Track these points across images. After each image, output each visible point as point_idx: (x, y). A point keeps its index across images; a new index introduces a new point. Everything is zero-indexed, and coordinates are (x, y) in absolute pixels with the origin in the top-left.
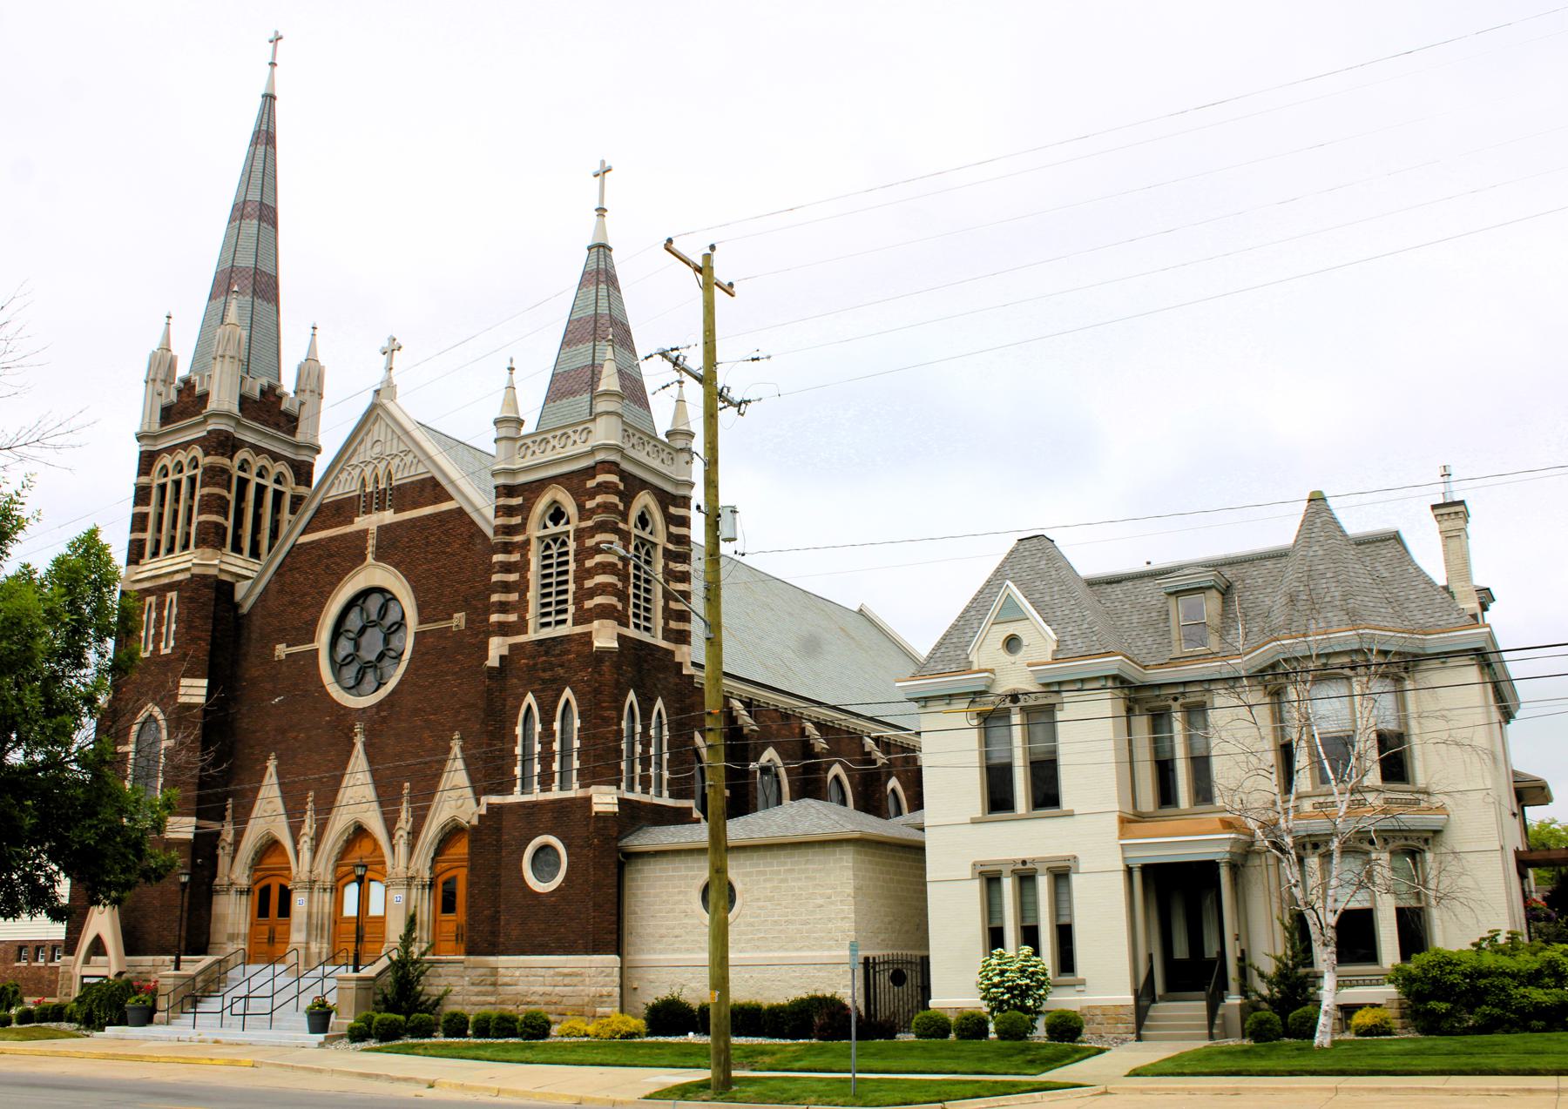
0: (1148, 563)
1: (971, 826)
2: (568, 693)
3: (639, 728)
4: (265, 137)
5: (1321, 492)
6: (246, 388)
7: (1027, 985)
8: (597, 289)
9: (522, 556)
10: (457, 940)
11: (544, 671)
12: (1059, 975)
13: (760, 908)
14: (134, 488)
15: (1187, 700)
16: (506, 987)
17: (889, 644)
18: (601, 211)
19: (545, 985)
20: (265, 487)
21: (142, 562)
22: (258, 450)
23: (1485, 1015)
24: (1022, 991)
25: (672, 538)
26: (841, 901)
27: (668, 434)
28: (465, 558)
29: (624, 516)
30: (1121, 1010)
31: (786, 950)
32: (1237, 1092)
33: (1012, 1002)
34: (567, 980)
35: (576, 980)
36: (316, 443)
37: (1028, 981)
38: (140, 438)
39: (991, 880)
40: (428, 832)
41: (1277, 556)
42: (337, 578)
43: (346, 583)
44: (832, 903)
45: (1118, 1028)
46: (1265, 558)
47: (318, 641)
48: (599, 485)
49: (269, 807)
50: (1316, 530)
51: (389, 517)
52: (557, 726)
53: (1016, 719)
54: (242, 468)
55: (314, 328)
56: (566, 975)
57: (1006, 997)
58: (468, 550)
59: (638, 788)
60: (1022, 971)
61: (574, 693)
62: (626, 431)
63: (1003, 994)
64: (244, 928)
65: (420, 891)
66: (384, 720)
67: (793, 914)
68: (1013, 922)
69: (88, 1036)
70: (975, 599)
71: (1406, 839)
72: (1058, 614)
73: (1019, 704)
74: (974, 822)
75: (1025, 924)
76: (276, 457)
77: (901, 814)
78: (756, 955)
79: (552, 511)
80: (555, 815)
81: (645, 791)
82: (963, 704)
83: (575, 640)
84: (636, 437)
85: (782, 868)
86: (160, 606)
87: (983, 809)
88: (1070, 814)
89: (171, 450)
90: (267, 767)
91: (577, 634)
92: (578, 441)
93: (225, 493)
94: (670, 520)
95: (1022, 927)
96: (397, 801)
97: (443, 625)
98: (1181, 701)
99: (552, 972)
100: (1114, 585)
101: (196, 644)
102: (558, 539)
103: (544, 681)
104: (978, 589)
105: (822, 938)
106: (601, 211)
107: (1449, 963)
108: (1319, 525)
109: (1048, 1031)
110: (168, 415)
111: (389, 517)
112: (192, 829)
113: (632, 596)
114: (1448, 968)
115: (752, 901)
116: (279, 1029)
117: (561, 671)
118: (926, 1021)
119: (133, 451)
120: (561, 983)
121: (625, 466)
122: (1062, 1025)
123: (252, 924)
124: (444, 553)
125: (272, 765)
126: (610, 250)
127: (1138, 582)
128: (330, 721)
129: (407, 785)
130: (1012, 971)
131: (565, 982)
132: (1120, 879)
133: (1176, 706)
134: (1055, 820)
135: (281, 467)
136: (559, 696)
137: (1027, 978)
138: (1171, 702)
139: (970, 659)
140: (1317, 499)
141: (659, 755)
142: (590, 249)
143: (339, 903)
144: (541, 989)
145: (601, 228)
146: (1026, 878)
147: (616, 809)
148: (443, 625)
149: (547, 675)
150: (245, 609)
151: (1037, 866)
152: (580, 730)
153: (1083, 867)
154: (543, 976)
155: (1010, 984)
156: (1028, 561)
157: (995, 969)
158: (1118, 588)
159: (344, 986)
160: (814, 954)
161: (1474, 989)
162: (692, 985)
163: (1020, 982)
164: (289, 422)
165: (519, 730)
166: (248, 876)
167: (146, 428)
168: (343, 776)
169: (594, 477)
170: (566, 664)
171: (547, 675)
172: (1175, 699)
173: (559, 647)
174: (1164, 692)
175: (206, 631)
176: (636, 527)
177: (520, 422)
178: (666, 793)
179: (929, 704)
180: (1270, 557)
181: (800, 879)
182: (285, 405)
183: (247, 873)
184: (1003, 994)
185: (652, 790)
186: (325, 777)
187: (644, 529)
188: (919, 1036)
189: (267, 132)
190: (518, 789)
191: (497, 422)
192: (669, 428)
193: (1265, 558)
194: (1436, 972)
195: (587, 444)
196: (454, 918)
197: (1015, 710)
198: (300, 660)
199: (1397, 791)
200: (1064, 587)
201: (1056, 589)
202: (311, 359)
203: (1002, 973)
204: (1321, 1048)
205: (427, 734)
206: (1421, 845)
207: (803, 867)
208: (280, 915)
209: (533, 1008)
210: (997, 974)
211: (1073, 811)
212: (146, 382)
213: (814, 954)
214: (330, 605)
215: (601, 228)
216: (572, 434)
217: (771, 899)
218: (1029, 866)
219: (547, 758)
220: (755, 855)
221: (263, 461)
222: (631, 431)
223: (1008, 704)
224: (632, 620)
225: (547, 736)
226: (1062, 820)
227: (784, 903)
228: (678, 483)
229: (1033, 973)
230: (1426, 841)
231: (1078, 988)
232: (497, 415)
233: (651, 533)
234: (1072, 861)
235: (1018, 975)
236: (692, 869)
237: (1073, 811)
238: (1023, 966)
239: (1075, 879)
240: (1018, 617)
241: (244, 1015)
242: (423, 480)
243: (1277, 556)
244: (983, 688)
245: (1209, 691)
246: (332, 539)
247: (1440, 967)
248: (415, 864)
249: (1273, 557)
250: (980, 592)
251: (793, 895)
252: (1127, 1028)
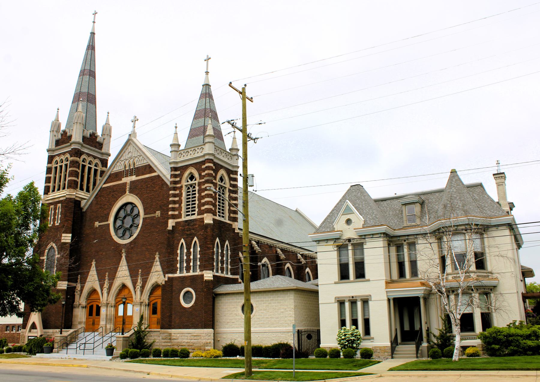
0: (396, 194)
1: (334, 284)
2: (195, 239)
3: (220, 251)
4: (91, 47)
5: (455, 170)
6: (85, 134)
7: (354, 339)
8: (206, 99)
9: (180, 191)
10: (157, 324)
11: (187, 231)
12: (365, 336)
13: (262, 313)
14: (46, 168)
15: (409, 241)
16: (174, 340)
17: (306, 222)
18: (207, 73)
19: (188, 339)
20: (91, 168)
21: (49, 193)
22: (89, 155)
23: (512, 350)
24: (352, 341)
25: (231, 185)
26: (290, 310)
27: (230, 150)
28: (160, 192)
29: (215, 178)
30: (386, 348)
31: (271, 327)
32: (426, 376)
34: (195, 338)
35: (198, 337)
36: (109, 153)
37: (354, 338)
38: (48, 151)
39: (341, 303)
40: (147, 286)
41: (440, 192)
42: (116, 199)
43: (119, 201)
44: (286, 311)
45: (385, 354)
46: (436, 192)
47: (110, 221)
48: (206, 167)
49: (93, 278)
51: (134, 178)
52: (192, 250)
53: (350, 247)
54: (83, 161)
55: (108, 113)
56: (195, 336)
57: (347, 343)
58: (161, 189)
59: (220, 271)
60: (352, 334)
61: (198, 239)
62: (215, 148)
63: (345, 342)
64: (84, 320)
65: (145, 307)
66: (132, 248)
67: (273, 315)
68: (349, 318)
69: (30, 357)
70: (336, 206)
71: (484, 289)
72: (364, 211)
73: (351, 243)
74: (336, 283)
75: (353, 318)
76: (95, 158)
77: (310, 280)
78: (260, 329)
79: (190, 176)
80: (191, 281)
81: (222, 272)
82: (332, 243)
83: (198, 220)
84: (219, 151)
85: (269, 299)
86: (55, 209)
87: (339, 279)
88: (369, 280)
89: (59, 155)
90: (92, 264)
91: (199, 218)
92: (199, 152)
93: (77, 170)
94: (231, 179)
95: (352, 319)
96: (137, 276)
97: (153, 215)
98: (407, 241)
99: (190, 335)
100: (384, 202)
101: (67, 222)
102: (192, 186)
103: (187, 235)
104: (337, 203)
105: (283, 323)
106: (207, 73)
107: (499, 332)
110: (58, 143)
111: (134, 178)
112: (66, 286)
113: (217, 205)
114: (499, 334)
115: (259, 310)
116: (96, 354)
117: (193, 231)
118: (319, 352)
119: (46, 155)
120: (193, 339)
121: (215, 160)
122: (366, 353)
123: (87, 318)
124: (153, 190)
125: (94, 263)
126: (210, 86)
127: (392, 201)
128: (114, 249)
129: (140, 270)
130: (348, 335)
131: (195, 338)
132: (386, 303)
133: (405, 243)
134: (363, 282)
135: (97, 161)
136: (192, 240)
137: (354, 337)
138: (403, 242)
139: (334, 227)
140: (453, 172)
141: (227, 260)
142: (203, 86)
143: (117, 311)
144: (186, 341)
145: (207, 79)
146: (353, 303)
147: (212, 279)
148: (153, 215)
149: (188, 233)
150: (84, 210)
151: (357, 298)
152: (200, 251)
153: (373, 299)
154: (187, 336)
155: (348, 339)
156: (354, 193)
157: (343, 334)
158: (385, 203)
159: (118, 340)
160: (280, 328)
161: (507, 341)
162: (238, 339)
163: (351, 338)
164: (100, 145)
165: (179, 252)
166: (85, 302)
167: (50, 147)
168: (118, 267)
169: (204, 164)
170: (195, 229)
171: (188, 233)
172: (405, 241)
173: (193, 223)
174: (401, 238)
175: (71, 217)
176: (219, 181)
177: (179, 145)
178: (229, 273)
179: (320, 242)
180: (437, 192)
181: (275, 303)
182: (98, 140)
183: (85, 301)
184: (345, 342)
185: (225, 272)
186: (112, 268)
187: (222, 182)
188: (316, 357)
189: (92, 45)
190: (178, 272)
191: (171, 145)
192: (230, 147)
193: (436, 192)
194: (494, 335)
195: (202, 153)
196: (156, 316)
198: (103, 227)
199: (481, 273)
200: (366, 202)
201: (364, 203)
202: (107, 124)
203: (345, 335)
204: (455, 361)
205: (147, 253)
206: (489, 291)
207: (277, 299)
208: (97, 315)
209: (183, 347)
210: (344, 336)
211: (369, 279)
212: (50, 132)
213: (280, 328)
214: (114, 209)
215: (207, 79)
216: (197, 149)
217: (265, 310)
218: (354, 298)
219: (188, 261)
220: (260, 294)
221: (91, 159)
222: (217, 148)
223: (347, 243)
224: (218, 213)
225: (188, 254)
226: (366, 282)
227: (270, 311)
228: (233, 166)
229: (356, 335)
231: (371, 340)
232: (171, 143)
233: (224, 184)
234: (369, 296)
235: (351, 336)
236: (238, 299)
237: (369, 279)
238: (352, 333)
239: (370, 303)
240: (350, 213)
241: (84, 349)
242: (146, 165)
243: (440, 192)
244: (338, 237)
245: (416, 238)
246: (114, 186)
248: (143, 298)
249: (438, 192)
250: (338, 204)
251: (273, 308)
252: (388, 354)
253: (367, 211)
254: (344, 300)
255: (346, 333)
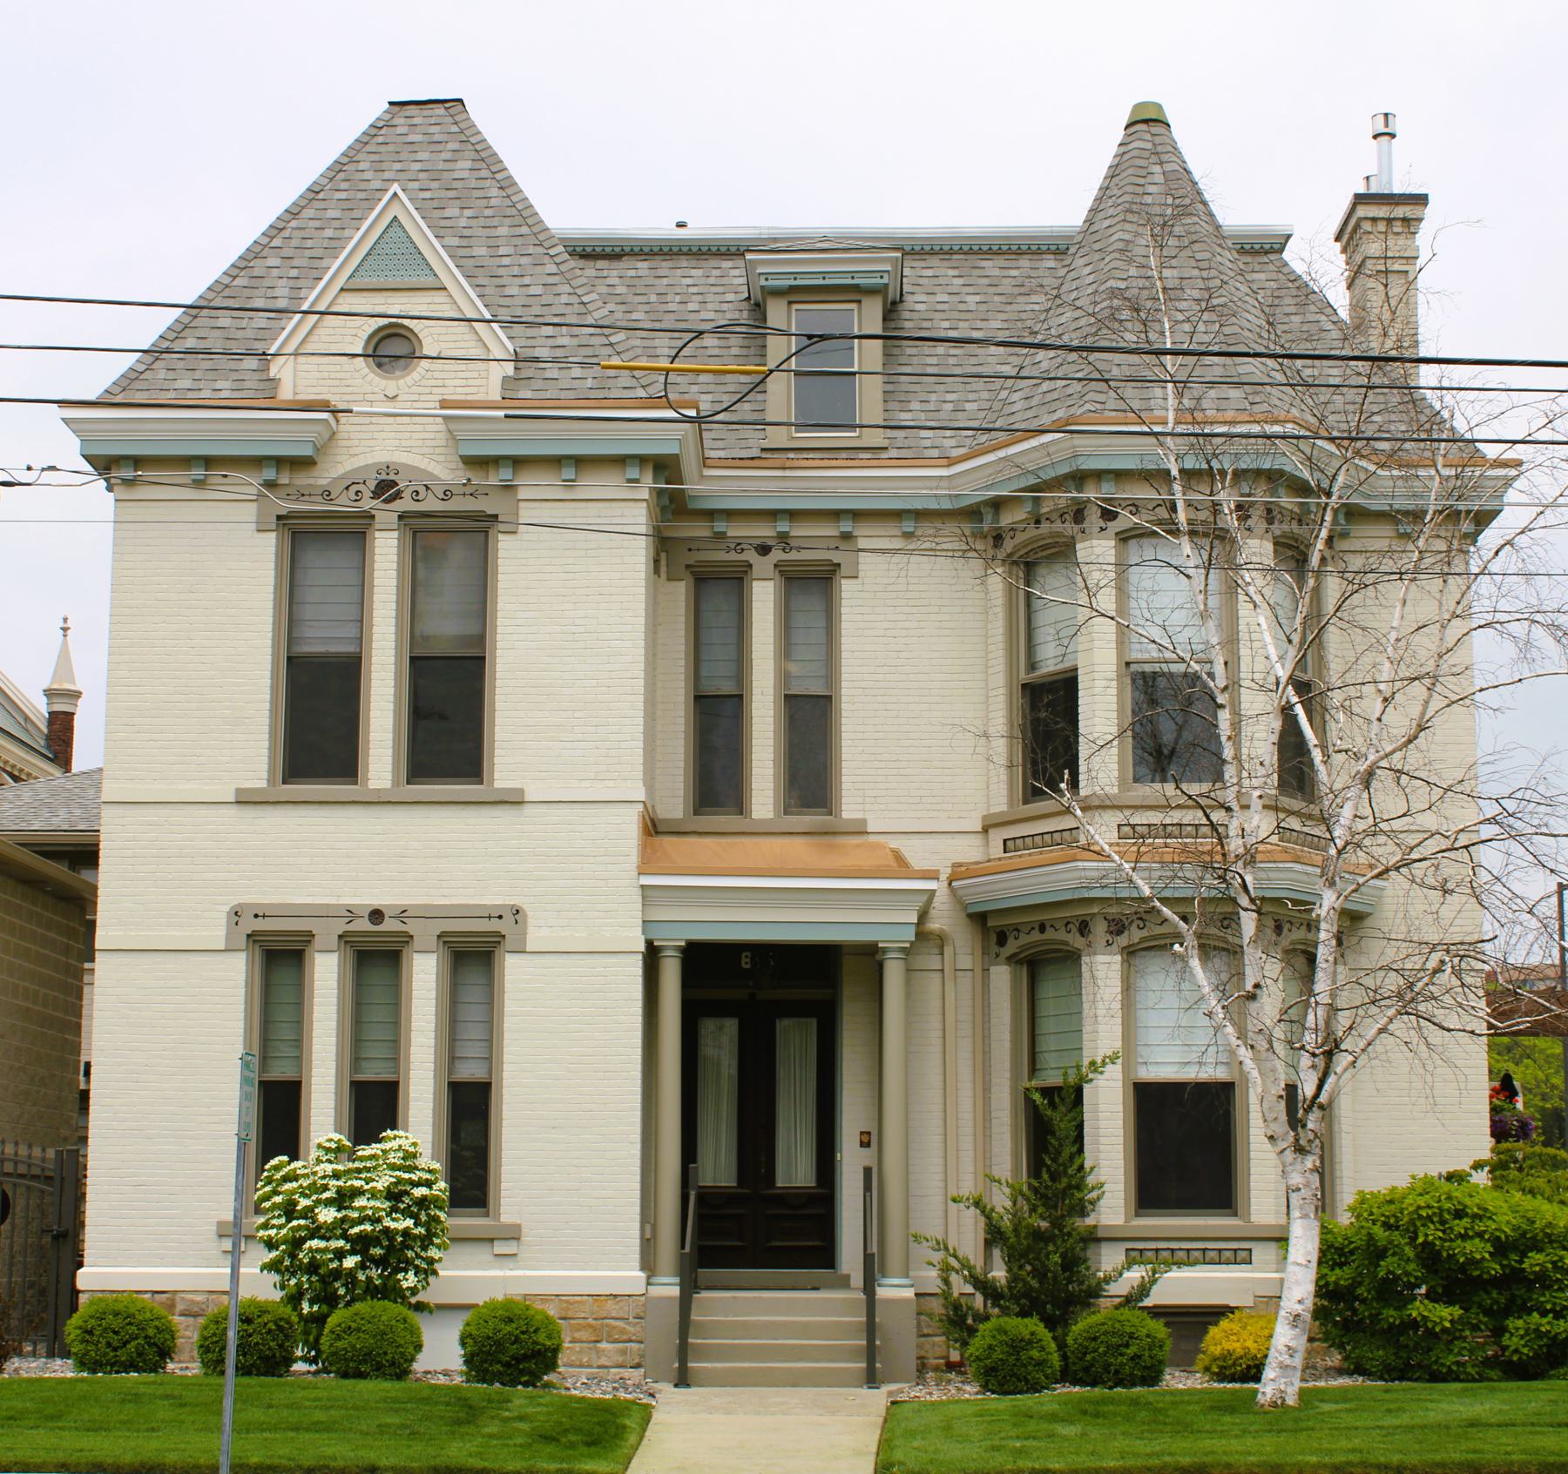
0: (681, 225)
1: (234, 811)
5: (1159, 107)
7: (406, 1233)
15: (793, 555)
23: (1539, 1334)
24: (390, 1249)
30: (612, 1308)
33: (361, 1277)
37: (409, 1222)
41: (1009, 252)
45: (599, 1352)
46: (980, 252)
50: (1152, 189)
53: (386, 549)
57: (350, 1262)
60: (394, 1195)
63: (340, 1255)
68: (332, 1071)
70: (275, 230)
72: (514, 291)
73: (400, 506)
74: (245, 800)
75: (366, 1076)
77: (1102, 516)
82: (250, 483)
87: (271, 771)
88: (513, 800)
95: (354, 1084)
98: (777, 555)
100: (601, 264)
104: (287, 204)
107: (1459, 1214)
108: (1159, 179)
109: (1330, 1297)
114: (1460, 1226)
118: (116, 1324)
122: (517, 1340)
127: (664, 266)
130: (374, 1195)
132: (634, 969)
133: (763, 565)
137: (407, 1213)
138: (751, 556)
139: (273, 373)
151: (411, 927)
155: (368, 1227)
156: (421, 156)
157: (325, 1188)
158: (613, 273)
161: (1514, 1278)
163: (393, 1225)
172: (764, 550)
174: (736, 531)
180: (990, 252)
184: (340, 1255)
188: (82, 1364)
193: (980, 252)
194: (1432, 1233)
197: (386, 515)
200: (525, 230)
201: (503, 231)
203: (343, 1199)
204: (1278, 1405)
210: (328, 1203)
218: (389, 925)
223: (367, 504)
226: (485, 812)
229: (423, 1202)
230: (1084, 928)
231: (500, 1248)
234: (508, 917)
235: (387, 1205)
237: (521, 791)
238: (399, 1181)
239: (513, 969)
240: (414, 281)
243: (1009, 252)
244: (307, 451)
245: (847, 537)
247: (1443, 1222)
249: (999, 253)
250: (292, 213)
252: (624, 1352)
253: (533, 290)
254: (310, 936)
255: (357, 1183)
